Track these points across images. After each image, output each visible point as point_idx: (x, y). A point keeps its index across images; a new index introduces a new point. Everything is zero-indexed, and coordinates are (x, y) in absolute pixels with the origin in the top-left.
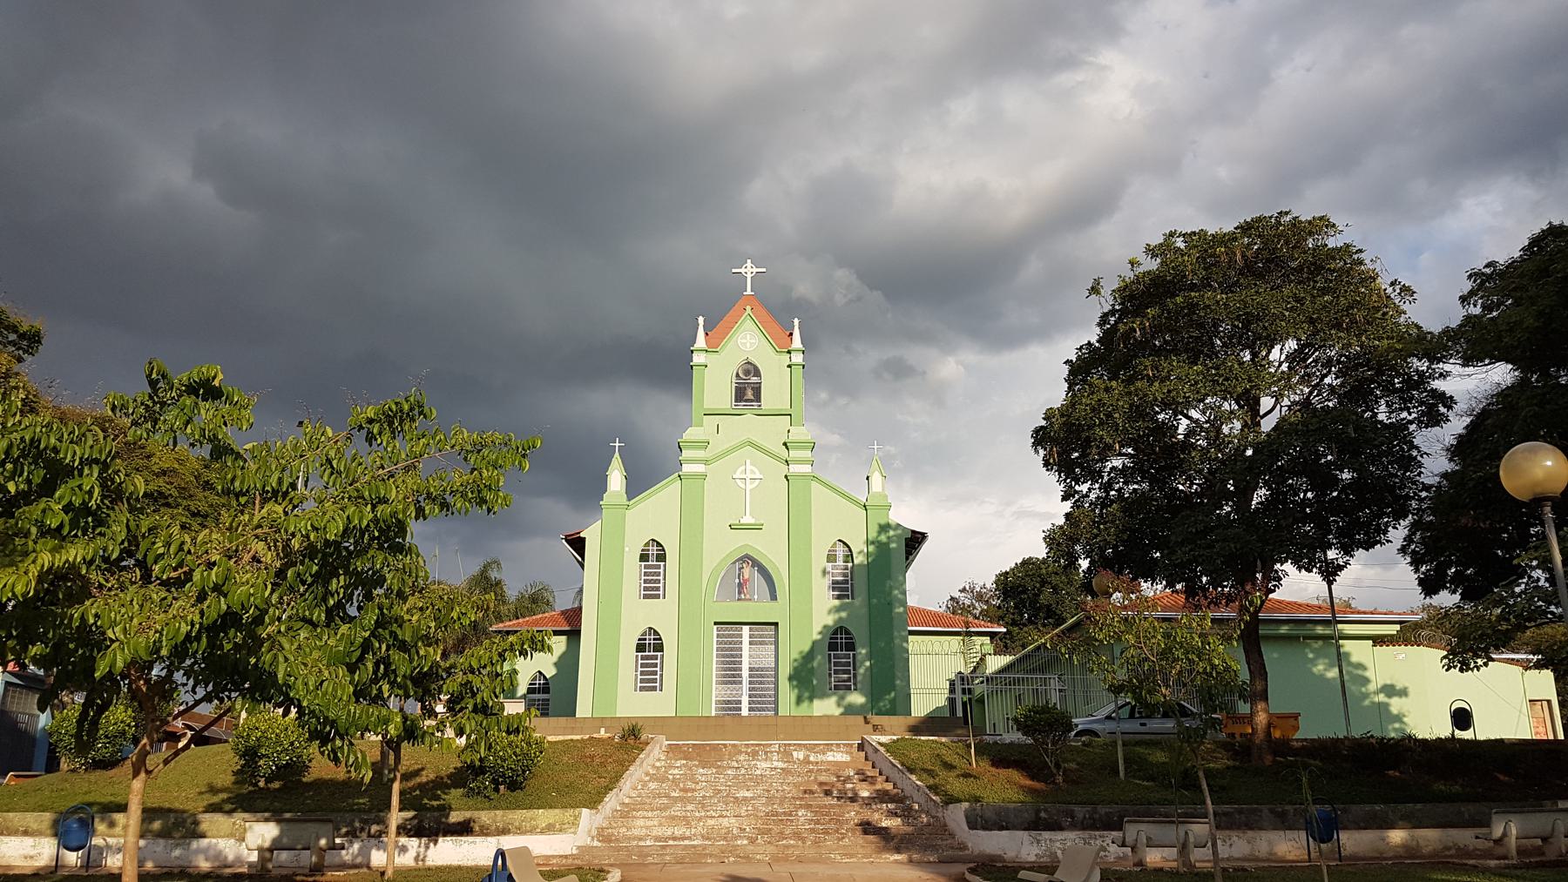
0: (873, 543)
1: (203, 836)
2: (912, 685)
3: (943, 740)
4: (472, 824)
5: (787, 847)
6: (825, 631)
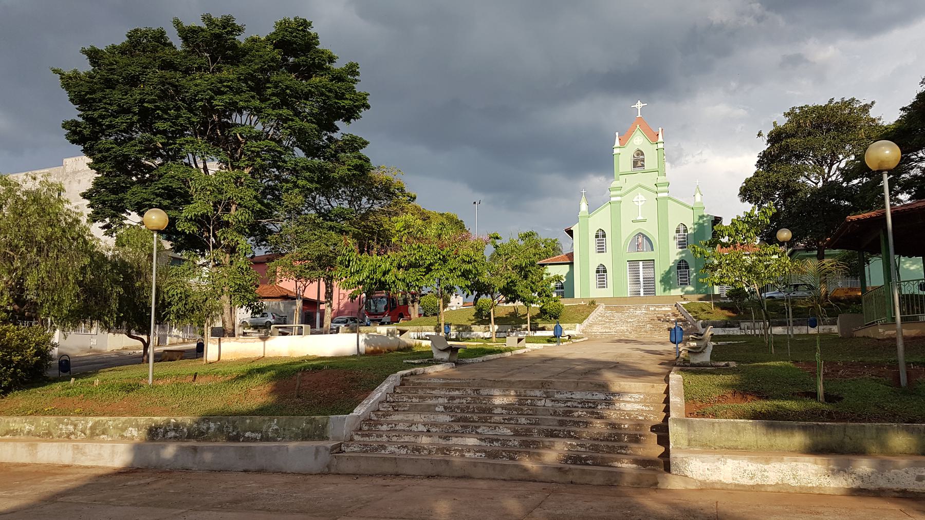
0: (696, 224)
1: (473, 331)
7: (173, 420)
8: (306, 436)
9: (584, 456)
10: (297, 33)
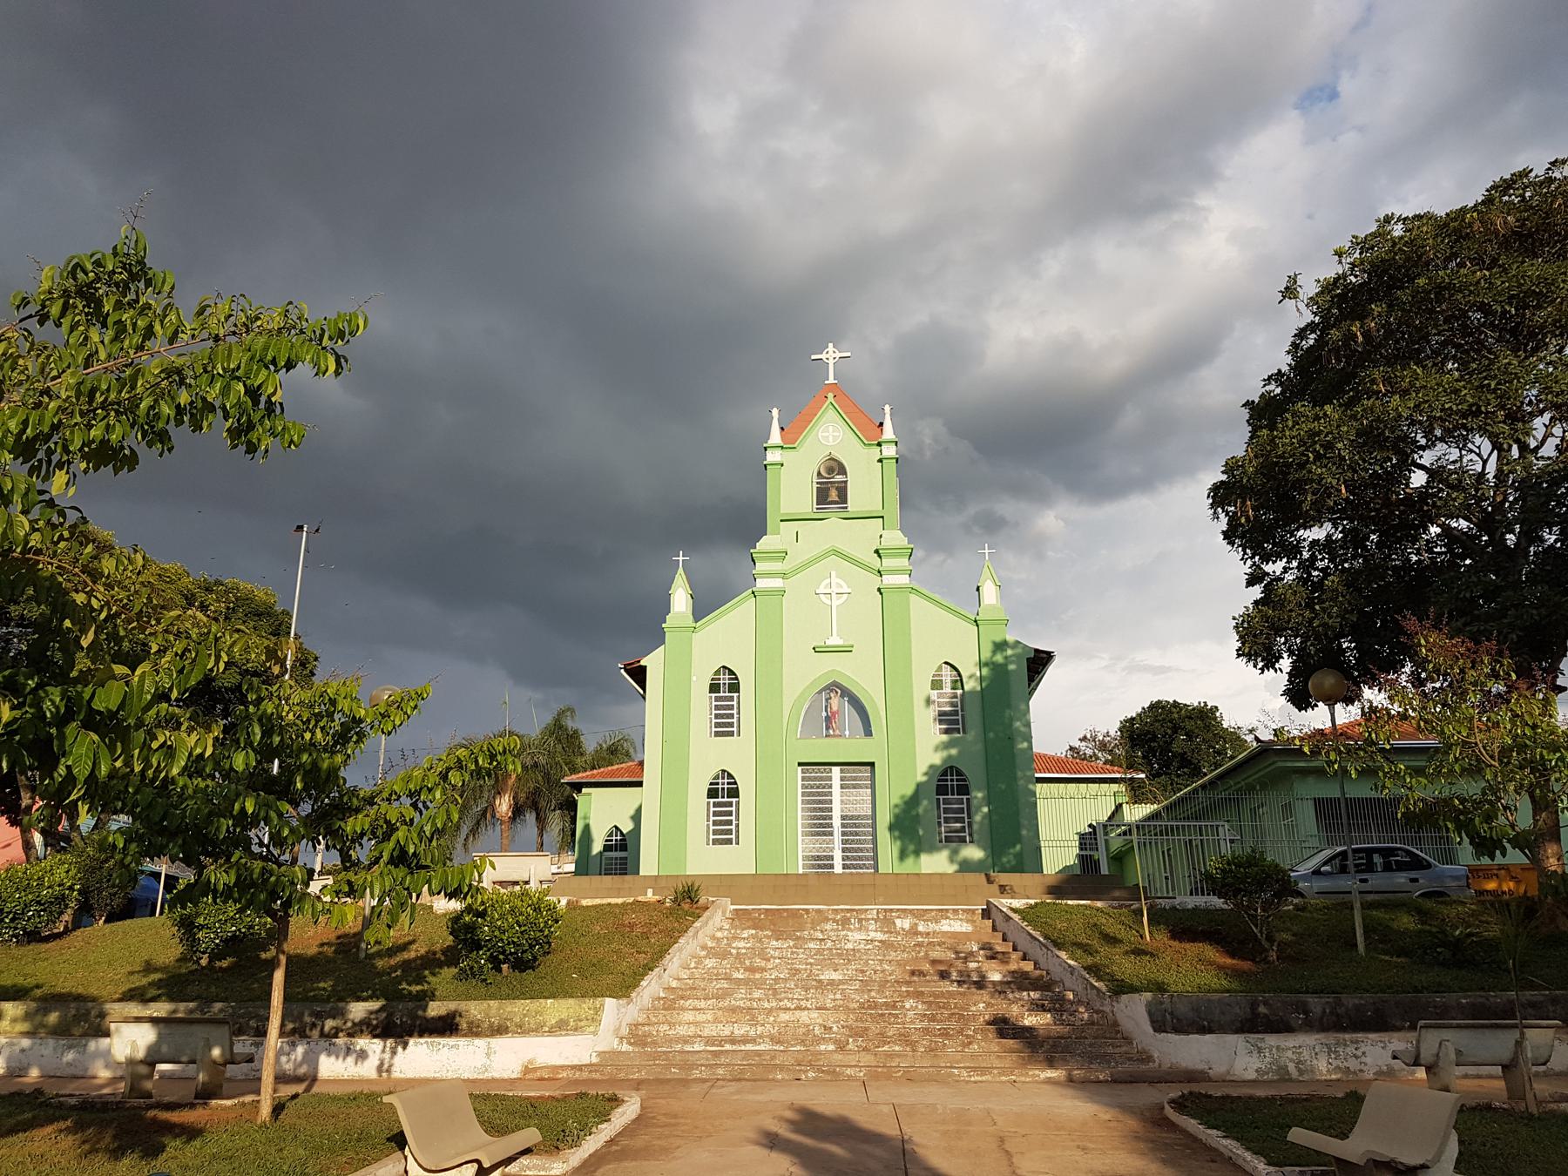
0: (986, 664)
2: (1042, 836)
3: (1099, 904)
4: (458, 1019)
5: (890, 1055)
6: (931, 772)
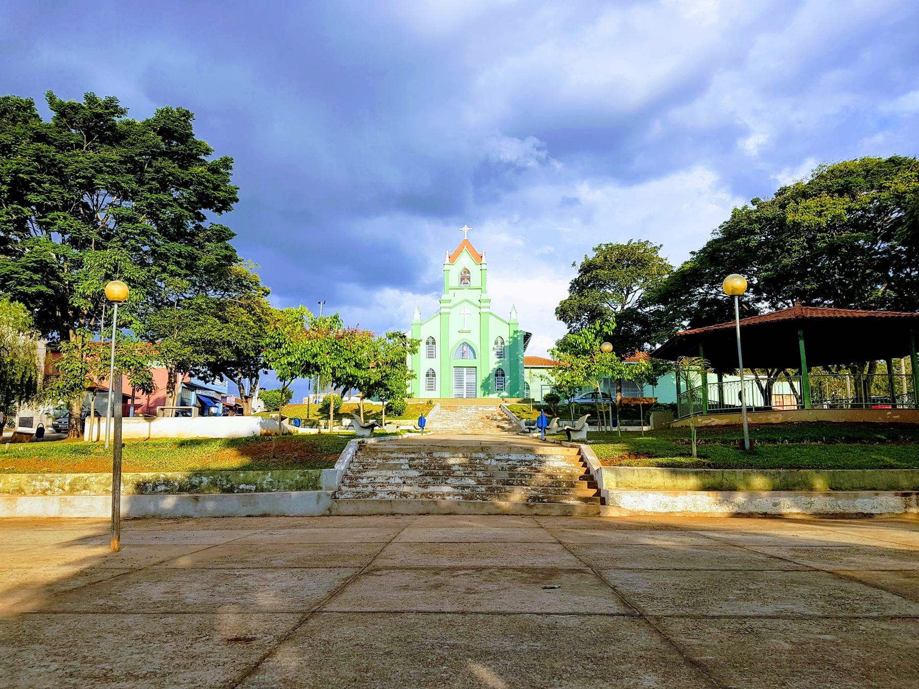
7: (162, 476)
8: (300, 487)
9: (541, 496)
10: (179, 123)
